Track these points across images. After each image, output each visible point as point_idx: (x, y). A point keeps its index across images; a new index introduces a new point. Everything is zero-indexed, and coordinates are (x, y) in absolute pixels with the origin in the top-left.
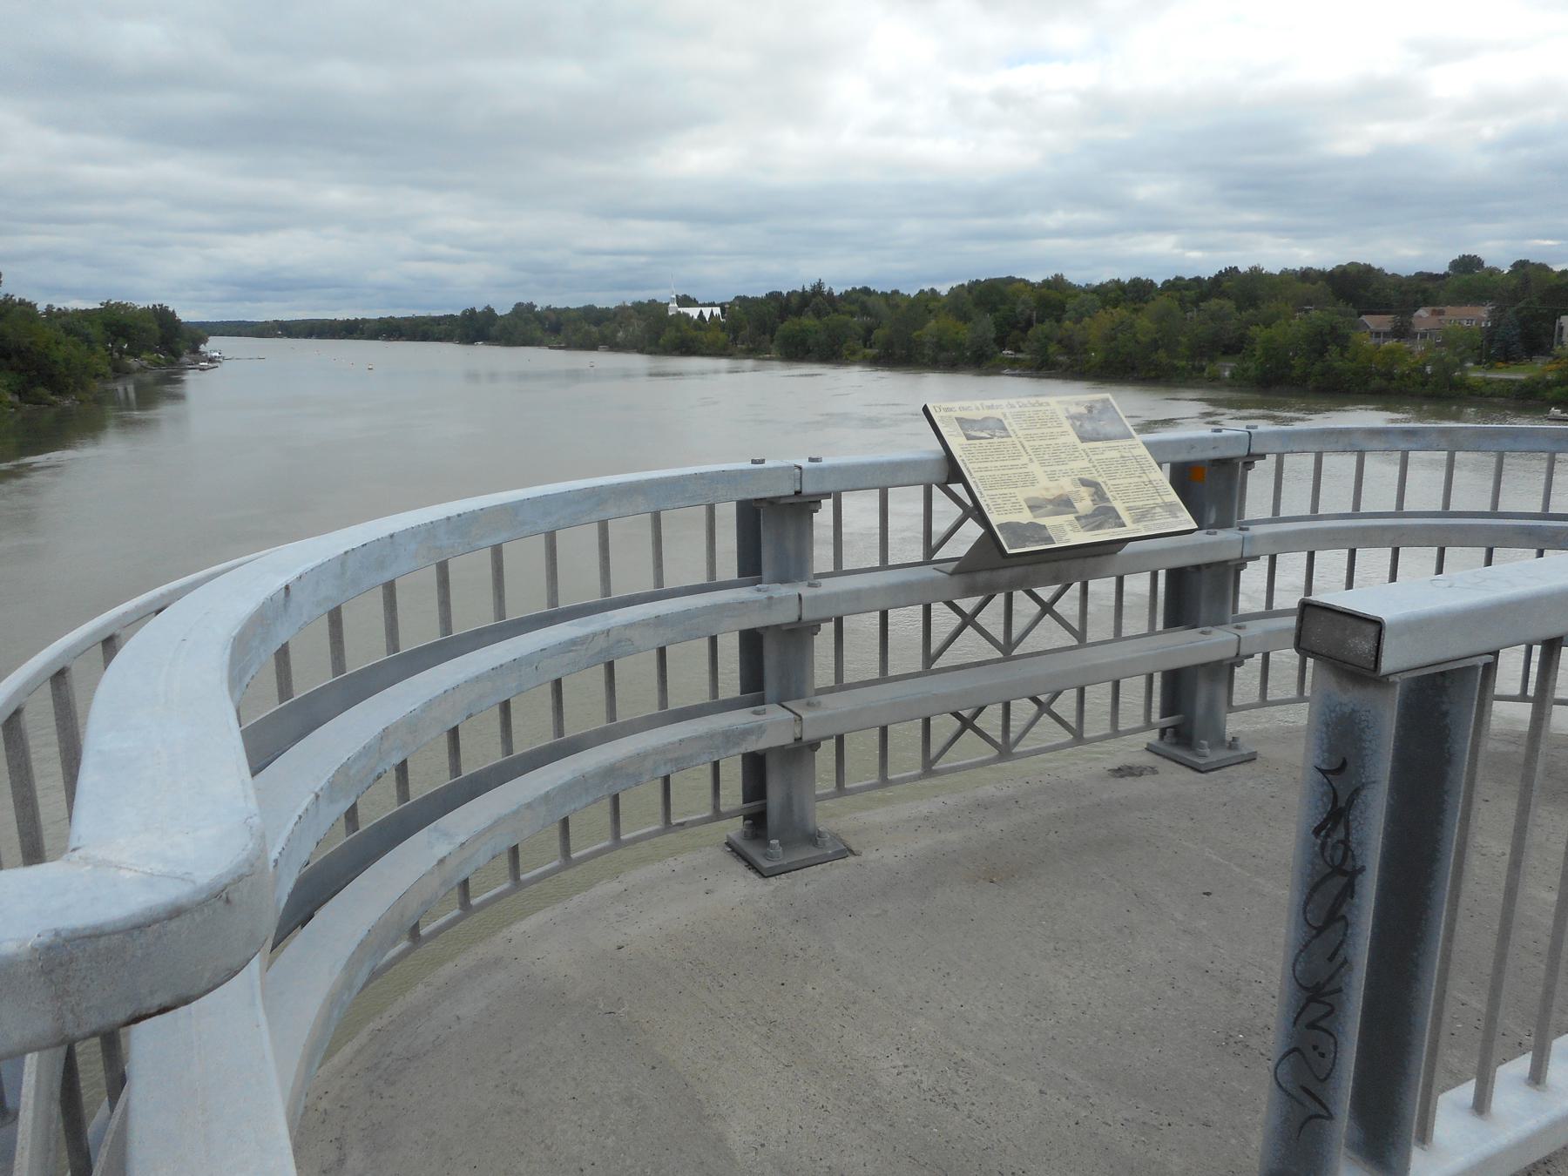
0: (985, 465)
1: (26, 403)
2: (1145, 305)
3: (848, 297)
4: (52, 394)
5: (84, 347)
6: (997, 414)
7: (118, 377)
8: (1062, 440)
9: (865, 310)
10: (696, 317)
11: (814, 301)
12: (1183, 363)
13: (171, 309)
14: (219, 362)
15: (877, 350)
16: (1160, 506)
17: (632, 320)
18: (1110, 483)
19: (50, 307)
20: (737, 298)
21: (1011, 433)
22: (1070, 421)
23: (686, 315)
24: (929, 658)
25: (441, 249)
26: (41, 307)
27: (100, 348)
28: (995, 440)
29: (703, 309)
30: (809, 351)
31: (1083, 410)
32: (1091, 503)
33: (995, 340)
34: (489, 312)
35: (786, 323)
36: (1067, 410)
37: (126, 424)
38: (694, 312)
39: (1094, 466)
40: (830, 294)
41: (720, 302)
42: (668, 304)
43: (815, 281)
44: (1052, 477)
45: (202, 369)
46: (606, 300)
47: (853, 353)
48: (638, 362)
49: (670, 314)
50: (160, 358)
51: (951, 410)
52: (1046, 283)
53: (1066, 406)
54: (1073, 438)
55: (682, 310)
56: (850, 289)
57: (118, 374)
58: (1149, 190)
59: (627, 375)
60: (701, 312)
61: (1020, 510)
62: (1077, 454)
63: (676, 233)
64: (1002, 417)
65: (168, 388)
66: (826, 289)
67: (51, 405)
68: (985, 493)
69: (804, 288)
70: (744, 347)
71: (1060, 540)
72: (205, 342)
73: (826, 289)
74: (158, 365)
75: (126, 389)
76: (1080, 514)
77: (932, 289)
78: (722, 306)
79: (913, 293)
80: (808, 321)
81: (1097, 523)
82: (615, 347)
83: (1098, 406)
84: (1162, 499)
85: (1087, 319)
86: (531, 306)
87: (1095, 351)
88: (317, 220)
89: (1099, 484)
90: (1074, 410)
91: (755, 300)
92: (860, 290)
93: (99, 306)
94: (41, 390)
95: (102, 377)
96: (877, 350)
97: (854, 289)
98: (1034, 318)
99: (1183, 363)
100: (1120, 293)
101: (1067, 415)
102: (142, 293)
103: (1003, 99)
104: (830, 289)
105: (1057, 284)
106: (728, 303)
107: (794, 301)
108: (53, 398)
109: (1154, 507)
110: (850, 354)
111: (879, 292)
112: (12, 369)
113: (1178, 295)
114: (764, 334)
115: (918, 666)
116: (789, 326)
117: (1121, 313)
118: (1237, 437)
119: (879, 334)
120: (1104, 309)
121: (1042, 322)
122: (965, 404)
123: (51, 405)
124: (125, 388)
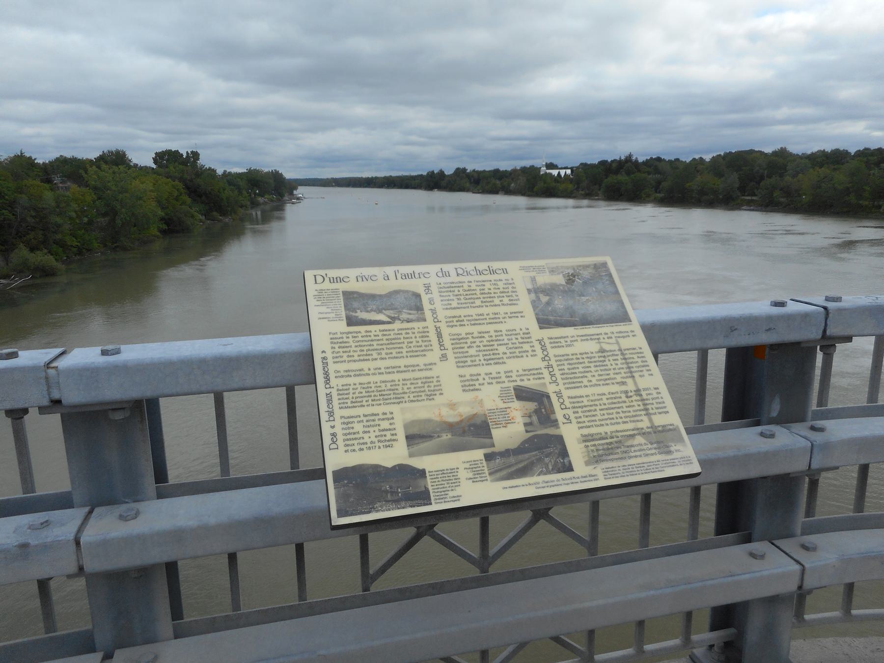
0: (365, 365)
1: (208, 220)
2: (841, 166)
3: (647, 163)
4: (220, 216)
5: (236, 192)
6: (416, 285)
7: (254, 207)
8: (512, 324)
9: (657, 171)
10: (556, 175)
11: (626, 165)
12: (867, 203)
13: (280, 172)
14: (302, 200)
15: (663, 195)
16: (643, 434)
17: (520, 177)
18: (566, 393)
19: (225, 171)
20: (582, 164)
21: (428, 314)
22: (533, 296)
23: (551, 174)
24: (368, 579)
25: (414, 138)
26: (220, 172)
27: (244, 192)
28: (397, 325)
29: (561, 171)
30: (621, 195)
31: (559, 280)
32: (522, 428)
33: (738, 188)
34: (441, 173)
35: (609, 179)
36: (533, 280)
37: (255, 232)
38: (555, 172)
39: (548, 367)
40: (636, 161)
41: (571, 166)
42: (541, 168)
43: (627, 154)
44: (469, 385)
45: (293, 203)
46: (505, 166)
47: (648, 196)
48: (521, 201)
49: (541, 173)
50: (273, 197)
51: (341, 280)
52: (775, 153)
53: (533, 274)
54: (530, 322)
55: (548, 171)
56: (649, 158)
57: (253, 206)
58: (847, 93)
59: (515, 208)
60: (559, 173)
61: (389, 444)
62: (526, 347)
63: (545, 127)
64: (421, 291)
65: (277, 214)
66: (634, 158)
67: (220, 221)
68: (338, 413)
69: (620, 158)
70: (583, 192)
71: (442, 498)
72: (296, 189)
73: (634, 158)
74: (272, 201)
75: (256, 213)
76: (496, 449)
77: (701, 158)
78: (572, 169)
79: (688, 160)
80: (622, 177)
81: (521, 465)
82: (508, 192)
83: (586, 274)
84: (651, 420)
85: (800, 175)
86: (464, 170)
87: (805, 194)
88: (350, 124)
89: (548, 397)
90: (544, 279)
91: (592, 166)
92: (655, 159)
93: (246, 171)
94: (215, 213)
95: (245, 207)
96: (663, 195)
97: (651, 158)
98: (765, 175)
99: (867, 203)
100: (824, 158)
101: (530, 286)
102: (266, 164)
103: (753, 37)
104: (636, 158)
105: (782, 154)
106: (576, 167)
107: (614, 165)
108: (221, 217)
109: (633, 436)
110: (646, 196)
111: (667, 160)
112: (202, 203)
113: (865, 159)
114: (595, 185)
115: (353, 585)
116: (611, 179)
117: (824, 171)
118: (806, 316)
119: (665, 185)
120: (813, 168)
121: (770, 177)
122: (367, 271)
123: (220, 221)
124: (257, 213)
